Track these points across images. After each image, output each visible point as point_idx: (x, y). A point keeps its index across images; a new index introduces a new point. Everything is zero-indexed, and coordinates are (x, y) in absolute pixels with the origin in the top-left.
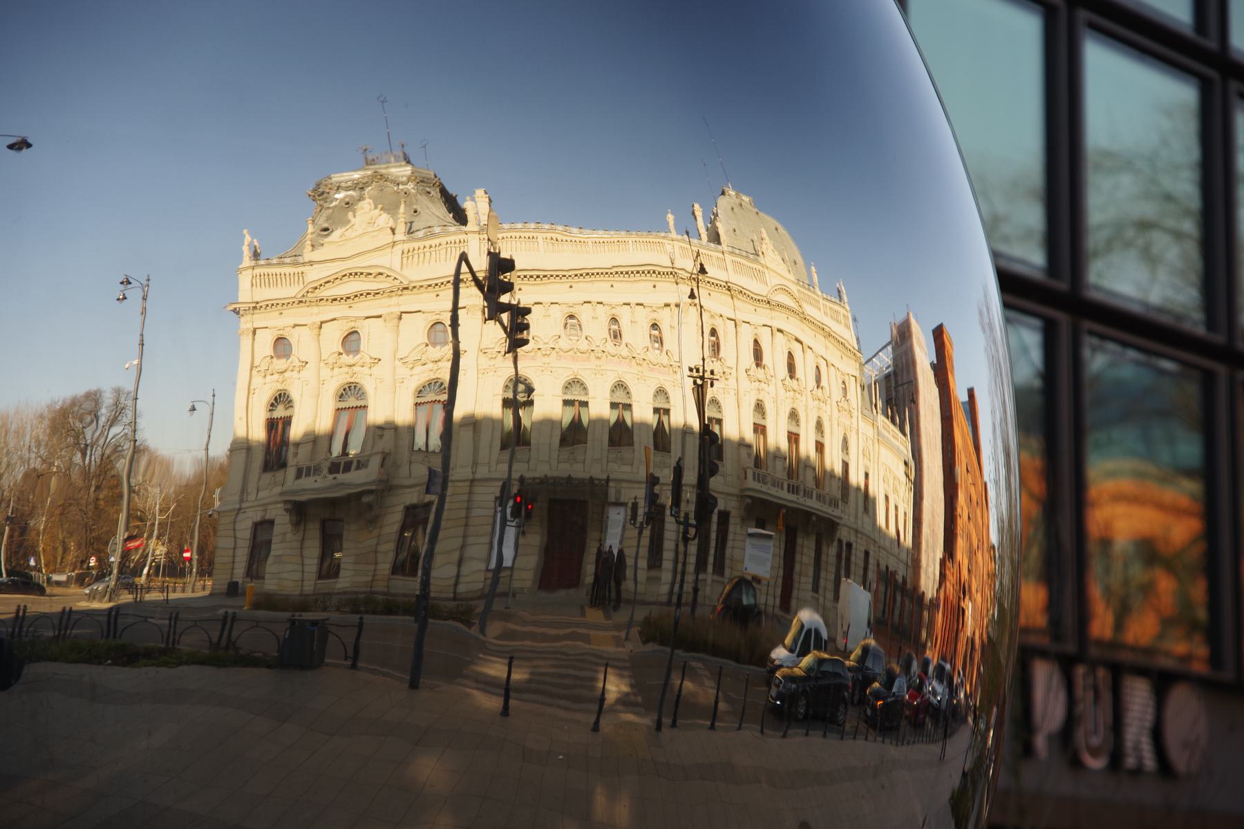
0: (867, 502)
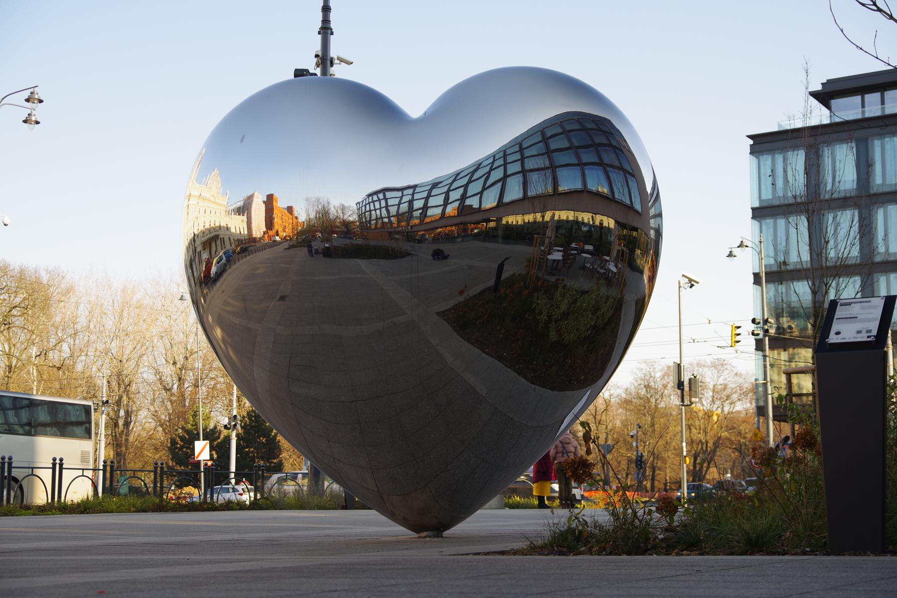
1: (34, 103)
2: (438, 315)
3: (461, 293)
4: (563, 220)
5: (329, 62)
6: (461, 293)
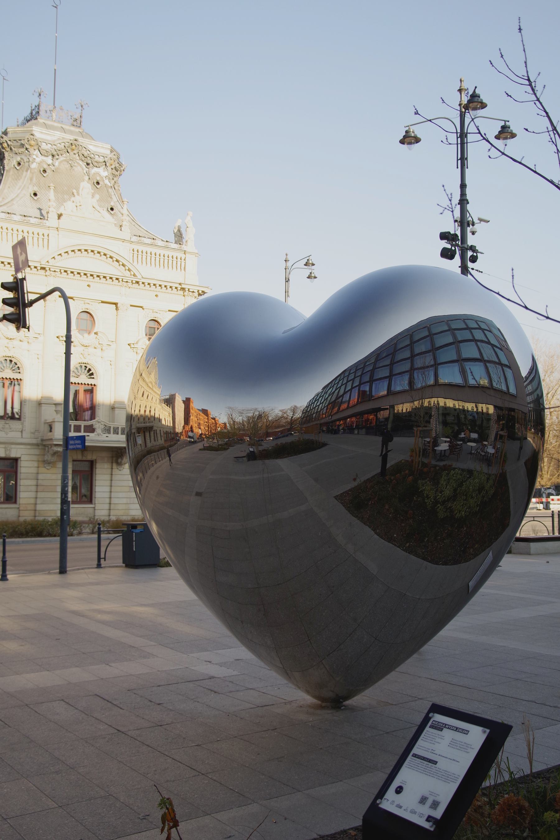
0: (160, 420)
1: (309, 266)
2: (336, 499)
3: (355, 480)
4: (449, 407)
5: (466, 224)
6: (355, 480)
